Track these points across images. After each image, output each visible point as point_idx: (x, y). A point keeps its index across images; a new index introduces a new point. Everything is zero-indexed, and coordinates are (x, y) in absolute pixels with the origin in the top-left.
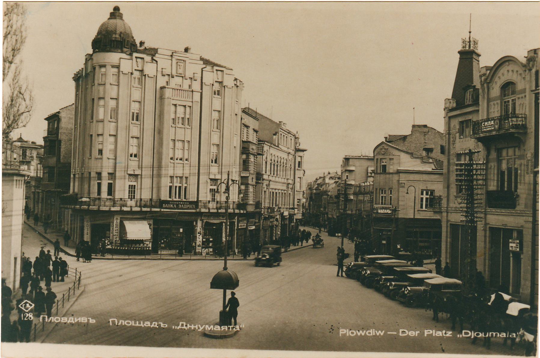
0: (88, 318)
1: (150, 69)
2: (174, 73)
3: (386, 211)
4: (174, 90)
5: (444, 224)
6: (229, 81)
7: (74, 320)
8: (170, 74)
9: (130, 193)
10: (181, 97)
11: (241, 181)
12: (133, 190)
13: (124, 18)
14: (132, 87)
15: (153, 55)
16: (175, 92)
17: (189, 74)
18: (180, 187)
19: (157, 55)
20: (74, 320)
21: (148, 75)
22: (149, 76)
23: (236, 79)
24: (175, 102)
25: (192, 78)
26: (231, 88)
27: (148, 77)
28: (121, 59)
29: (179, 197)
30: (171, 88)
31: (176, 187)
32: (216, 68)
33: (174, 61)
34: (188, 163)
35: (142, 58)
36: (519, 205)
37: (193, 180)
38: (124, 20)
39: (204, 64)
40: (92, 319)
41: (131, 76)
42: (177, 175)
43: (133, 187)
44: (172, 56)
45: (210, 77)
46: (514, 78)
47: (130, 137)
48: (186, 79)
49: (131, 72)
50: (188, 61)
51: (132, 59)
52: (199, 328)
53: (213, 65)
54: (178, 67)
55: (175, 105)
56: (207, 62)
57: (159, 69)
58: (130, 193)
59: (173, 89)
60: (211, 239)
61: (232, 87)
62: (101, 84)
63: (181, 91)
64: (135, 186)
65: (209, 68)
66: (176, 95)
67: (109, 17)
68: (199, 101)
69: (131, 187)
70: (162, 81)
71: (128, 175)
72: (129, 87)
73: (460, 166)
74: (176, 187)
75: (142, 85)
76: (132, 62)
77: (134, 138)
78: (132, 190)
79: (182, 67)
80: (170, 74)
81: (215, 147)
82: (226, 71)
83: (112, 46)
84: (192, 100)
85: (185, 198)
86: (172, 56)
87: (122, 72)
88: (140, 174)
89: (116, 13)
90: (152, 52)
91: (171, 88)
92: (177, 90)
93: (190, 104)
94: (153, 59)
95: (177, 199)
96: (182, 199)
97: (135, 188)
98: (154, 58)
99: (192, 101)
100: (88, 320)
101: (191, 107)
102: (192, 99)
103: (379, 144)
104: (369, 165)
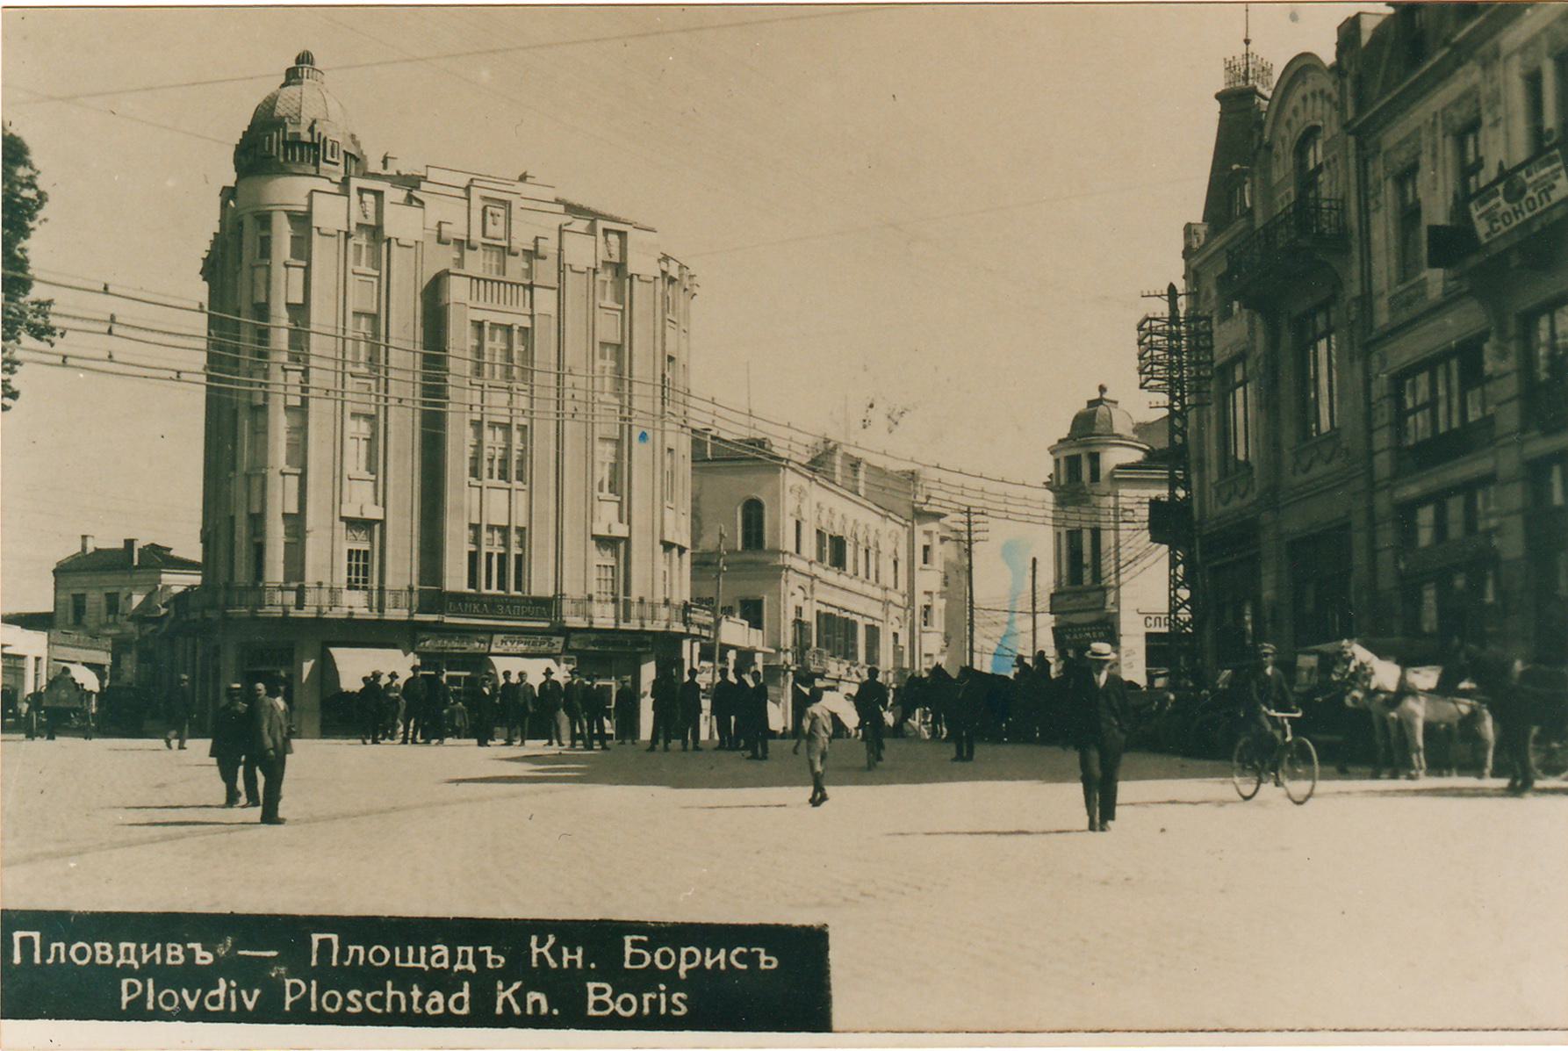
0: (190, 945)
1: (401, 222)
2: (476, 237)
4: (475, 281)
5: (717, 660)
7: (138, 956)
8: (465, 238)
9: (353, 571)
10: (498, 302)
12: (361, 563)
14: (597, 308)
16: (492, 287)
17: (521, 240)
18: (503, 559)
20: (138, 956)
21: (397, 239)
22: (574, 268)
23: (666, 258)
24: (479, 316)
25: (462, 241)
26: (649, 282)
27: (399, 245)
28: (315, 194)
29: (501, 586)
30: (467, 276)
31: (489, 555)
32: (601, 224)
33: (477, 205)
34: (524, 487)
37: (542, 539)
40: (204, 949)
41: (594, 277)
42: (493, 522)
43: (354, 556)
44: (467, 189)
47: (596, 438)
48: (475, 249)
49: (346, 230)
50: (517, 203)
53: (594, 216)
54: (489, 219)
55: (479, 326)
56: (573, 209)
57: (432, 225)
58: (353, 571)
59: (472, 278)
60: (1191, 684)
61: (655, 278)
63: (495, 284)
64: (366, 552)
66: (495, 300)
67: (283, 79)
68: (554, 313)
69: (354, 556)
70: (442, 259)
71: (344, 524)
72: (590, 306)
74: (489, 555)
75: (379, 269)
76: (349, 201)
77: (362, 420)
78: (357, 566)
79: (501, 220)
80: (465, 238)
81: (499, 433)
82: (633, 236)
83: (289, 158)
84: (532, 311)
85: (518, 587)
86: (467, 189)
87: (318, 228)
88: (381, 517)
91: (467, 276)
92: (485, 281)
93: (527, 323)
95: (494, 590)
96: (508, 592)
97: (365, 559)
98: (416, 193)
100: (190, 954)
101: (530, 332)
102: (532, 306)
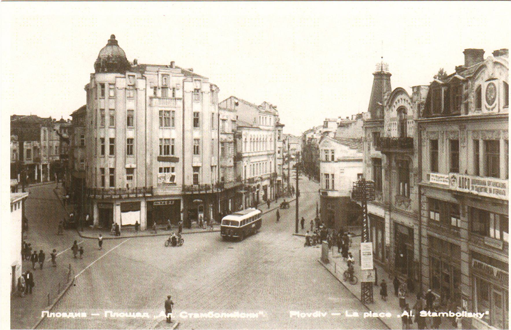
3: (416, 252)
6: (206, 88)
11: (436, 238)
13: (119, 44)
15: (142, 73)
19: (146, 72)
33: (160, 76)
35: (134, 76)
36: (351, 246)
38: (119, 46)
39: (185, 76)
45: (190, 86)
46: (405, 104)
51: (125, 77)
52: (479, 316)
62: (137, 133)
65: (189, 79)
73: (482, 265)
89: (113, 42)
90: (142, 69)
94: (142, 76)
98: (143, 75)
99: (126, 90)
103: (508, 96)
104: (99, 251)
